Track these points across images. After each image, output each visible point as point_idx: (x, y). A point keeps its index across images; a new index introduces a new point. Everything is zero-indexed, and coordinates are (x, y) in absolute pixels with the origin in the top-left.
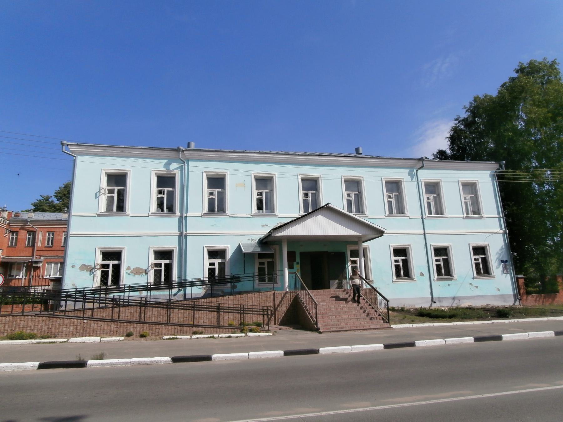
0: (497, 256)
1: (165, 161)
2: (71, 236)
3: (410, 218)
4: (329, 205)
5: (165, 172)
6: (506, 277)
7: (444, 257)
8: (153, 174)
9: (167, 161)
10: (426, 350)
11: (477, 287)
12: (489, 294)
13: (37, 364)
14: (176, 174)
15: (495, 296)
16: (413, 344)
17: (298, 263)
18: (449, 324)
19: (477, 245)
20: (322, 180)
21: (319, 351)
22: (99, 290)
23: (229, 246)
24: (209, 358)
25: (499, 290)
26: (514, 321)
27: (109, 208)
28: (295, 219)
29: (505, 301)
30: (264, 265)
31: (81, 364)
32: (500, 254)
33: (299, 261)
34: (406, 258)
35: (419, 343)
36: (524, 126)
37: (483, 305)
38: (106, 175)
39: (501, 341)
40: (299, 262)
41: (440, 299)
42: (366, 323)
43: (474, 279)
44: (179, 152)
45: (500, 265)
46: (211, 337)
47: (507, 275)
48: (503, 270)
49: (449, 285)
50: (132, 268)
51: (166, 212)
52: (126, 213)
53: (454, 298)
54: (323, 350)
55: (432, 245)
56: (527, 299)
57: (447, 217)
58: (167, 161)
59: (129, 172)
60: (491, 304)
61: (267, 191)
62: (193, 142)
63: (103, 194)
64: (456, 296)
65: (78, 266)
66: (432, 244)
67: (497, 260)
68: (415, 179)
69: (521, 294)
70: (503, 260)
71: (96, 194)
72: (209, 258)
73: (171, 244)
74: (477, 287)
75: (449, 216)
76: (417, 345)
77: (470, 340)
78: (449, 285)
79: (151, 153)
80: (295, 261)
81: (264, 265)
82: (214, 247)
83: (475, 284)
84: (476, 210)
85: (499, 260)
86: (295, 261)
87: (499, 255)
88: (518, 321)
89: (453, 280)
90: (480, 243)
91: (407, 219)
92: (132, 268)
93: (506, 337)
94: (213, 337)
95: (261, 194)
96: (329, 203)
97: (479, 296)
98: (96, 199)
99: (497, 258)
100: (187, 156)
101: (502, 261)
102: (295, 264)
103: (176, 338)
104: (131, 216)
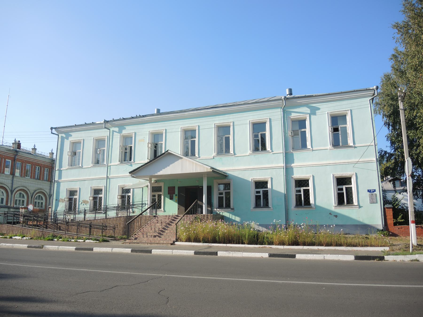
4: (169, 151)
20: (214, 127)
21: (93, 249)
28: (144, 164)
30: (155, 197)
33: (177, 194)
35: (154, 251)
40: (177, 194)
54: (155, 252)
70: (370, 190)
72: (351, 187)
73: (101, 185)
77: (130, 250)
79: (135, 120)
80: (175, 194)
81: (155, 197)
84: (126, 153)
86: (175, 194)
96: (168, 150)
102: (174, 195)
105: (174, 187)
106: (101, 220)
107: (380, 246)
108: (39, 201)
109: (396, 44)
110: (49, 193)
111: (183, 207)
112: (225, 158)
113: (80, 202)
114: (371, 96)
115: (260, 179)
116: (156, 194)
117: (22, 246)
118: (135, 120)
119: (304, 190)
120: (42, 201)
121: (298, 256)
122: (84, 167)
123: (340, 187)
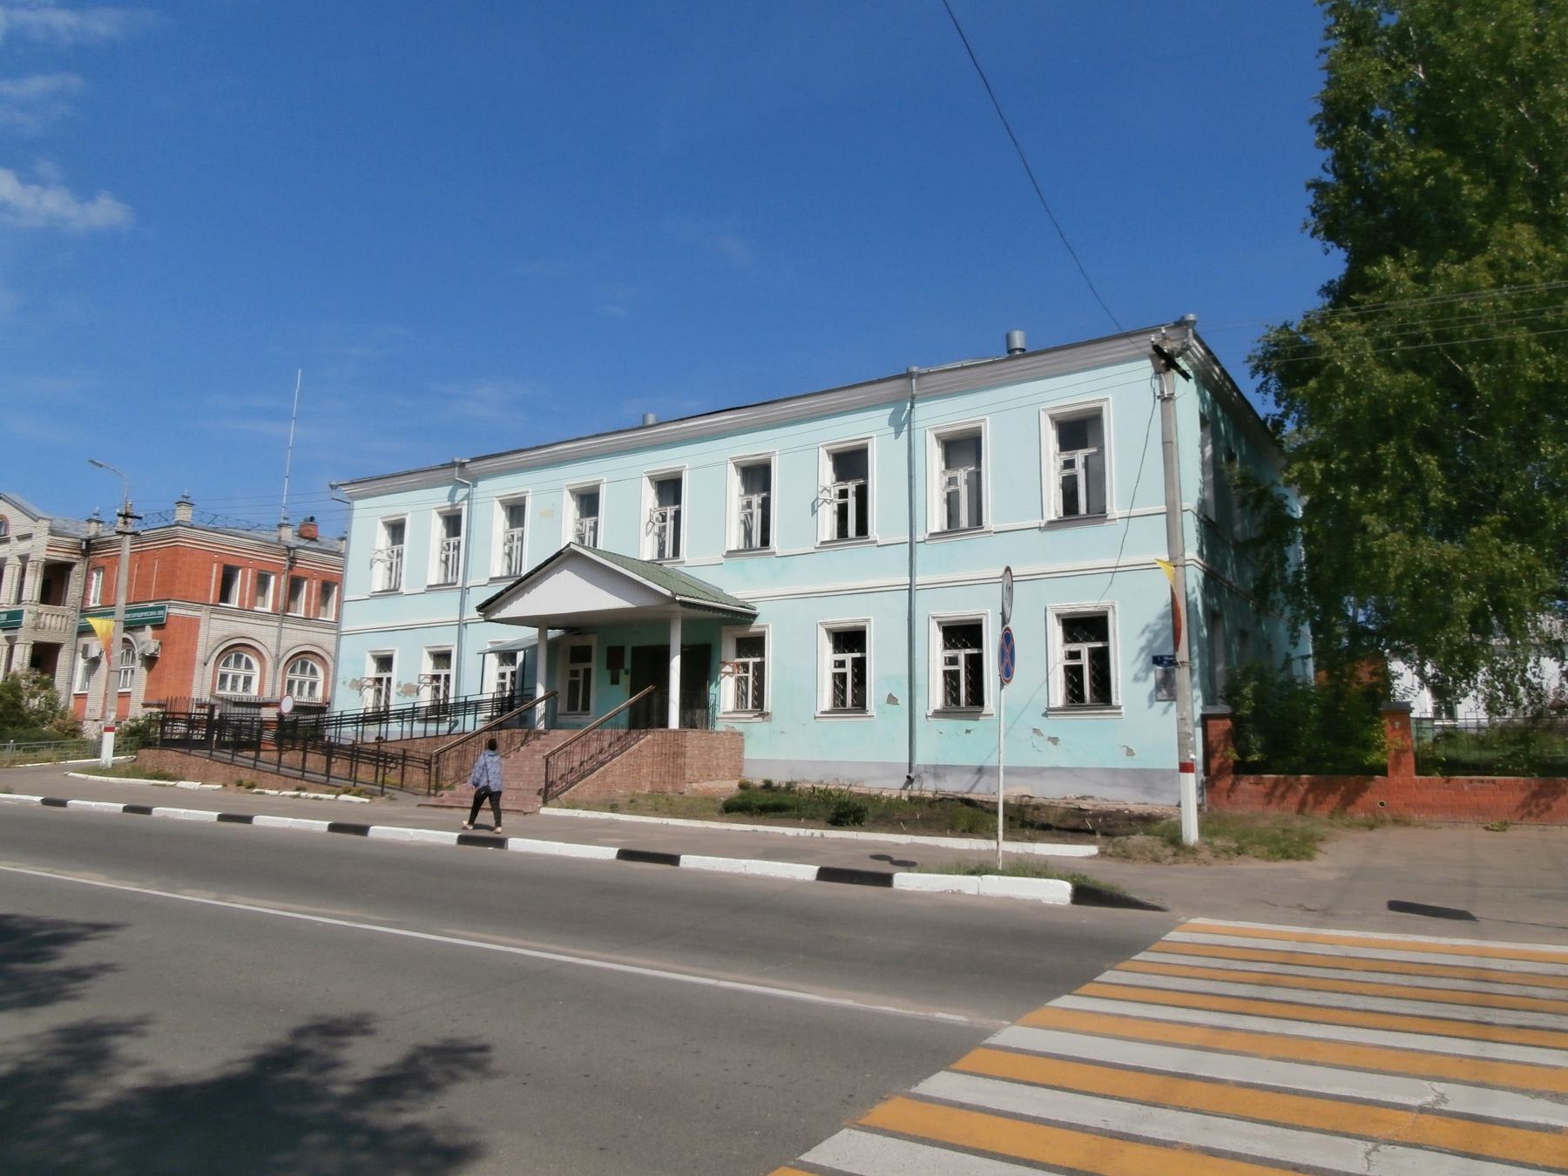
0: (1143, 641)
1: (890, 411)
2: (918, 588)
3: (878, 546)
5: (449, 509)
6: (1166, 711)
7: (969, 651)
8: (823, 452)
9: (892, 410)
10: (165, 821)
11: (1054, 740)
12: (1092, 762)
13: (216, 814)
14: (980, 427)
15: (1113, 772)
16: (673, 860)
17: (626, 673)
18: (639, 821)
19: (1073, 610)
22: (1432, 720)
23: (989, 612)
24: (63, 804)
25: (1130, 752)
26: (813, 834)
27: (842, 532)
29: (1149, 789)
31: (147, 811)
32: (1156, 634)
34: (863, 655)
36: (1541, 99)
37: (1068, 796)
38: (737, 472)
39: (676, 867)
41: (937, 771)
42: (514, 798)
43: (1050, 717)
44: (1187, 331)
45: (1148, 670)
46: (294, 797)
47: (1170, 705)
48: (1158, 687)
49: (968, 731)
50: (403, 684)
51: (214, 601)
52: (1106, 516)
53: (980, 771)
55: (933, 618)
56: (1232, 789)
57: (990, 532)
58: (892, 410)
59: (983, 424)
60: (1096, 795)
61: (1086, 451)
62: (1017, 329)
63: (825, 500)
64: (985, 765)
65: (348, 683)
66: (933, 613)
67: (1143, 656)
68: (904, 434)
69: (1213, 772)
70: (1162, 657)
71: (813, 504)
74: (1054, 740)
75: (994, 528)
76: (682, 864)
77: (808, 872)
78: (968, 731)
81: (844, 666)
82: (501, 642)
83: (1048, 733)
85: (1147, 655)
87: (1152, 636)
88: (822, 836)
89: (980, 718)
90: (1085, 603)
91: (873, 549)
92: (403, 684)
93: (260, 821)
94: (298, 796)
95: (749, 505)
97: (1060, 768)
98: (812, 515)
99: (1142, 649)
100: (470, 470)
101: (1157, 660)
102: (622, 672)
103: (263, 793)
104: (995, 533)
105: (621, 649)
106: (668, 735)
107: (749, 510)
108: (237, 672)
109: (1317, 53)
110: (273, 650)
111: (546, 692)
112: (755, 564)
113: (1213, 757)
114: (975, 1058)
115: (843, 625)
116: (581, 667)
117: (96, 806)
118: (1445, 941)
119: (969, 658)
120: (248, 673)
121: (904, 880)
122: (403, 589)
123: (1074, 647)
